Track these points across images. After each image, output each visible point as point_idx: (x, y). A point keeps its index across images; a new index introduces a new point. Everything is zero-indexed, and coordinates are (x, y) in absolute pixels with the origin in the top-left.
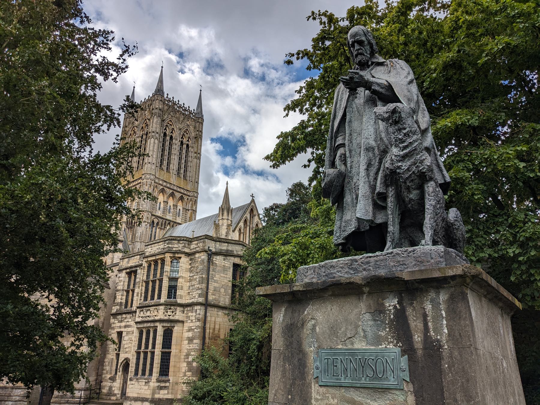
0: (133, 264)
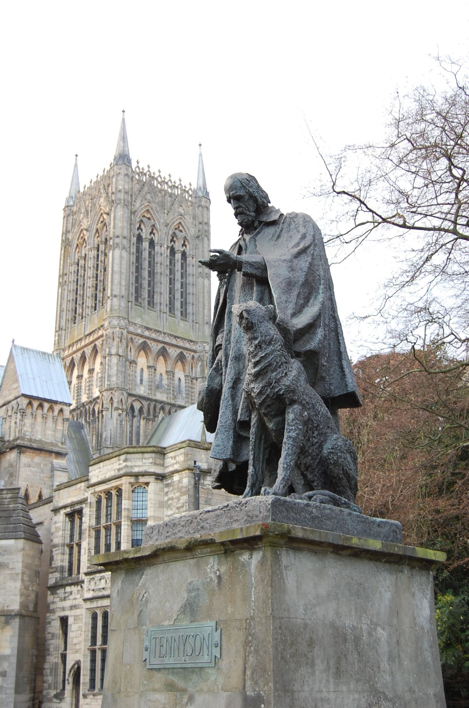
0: (75, 499)
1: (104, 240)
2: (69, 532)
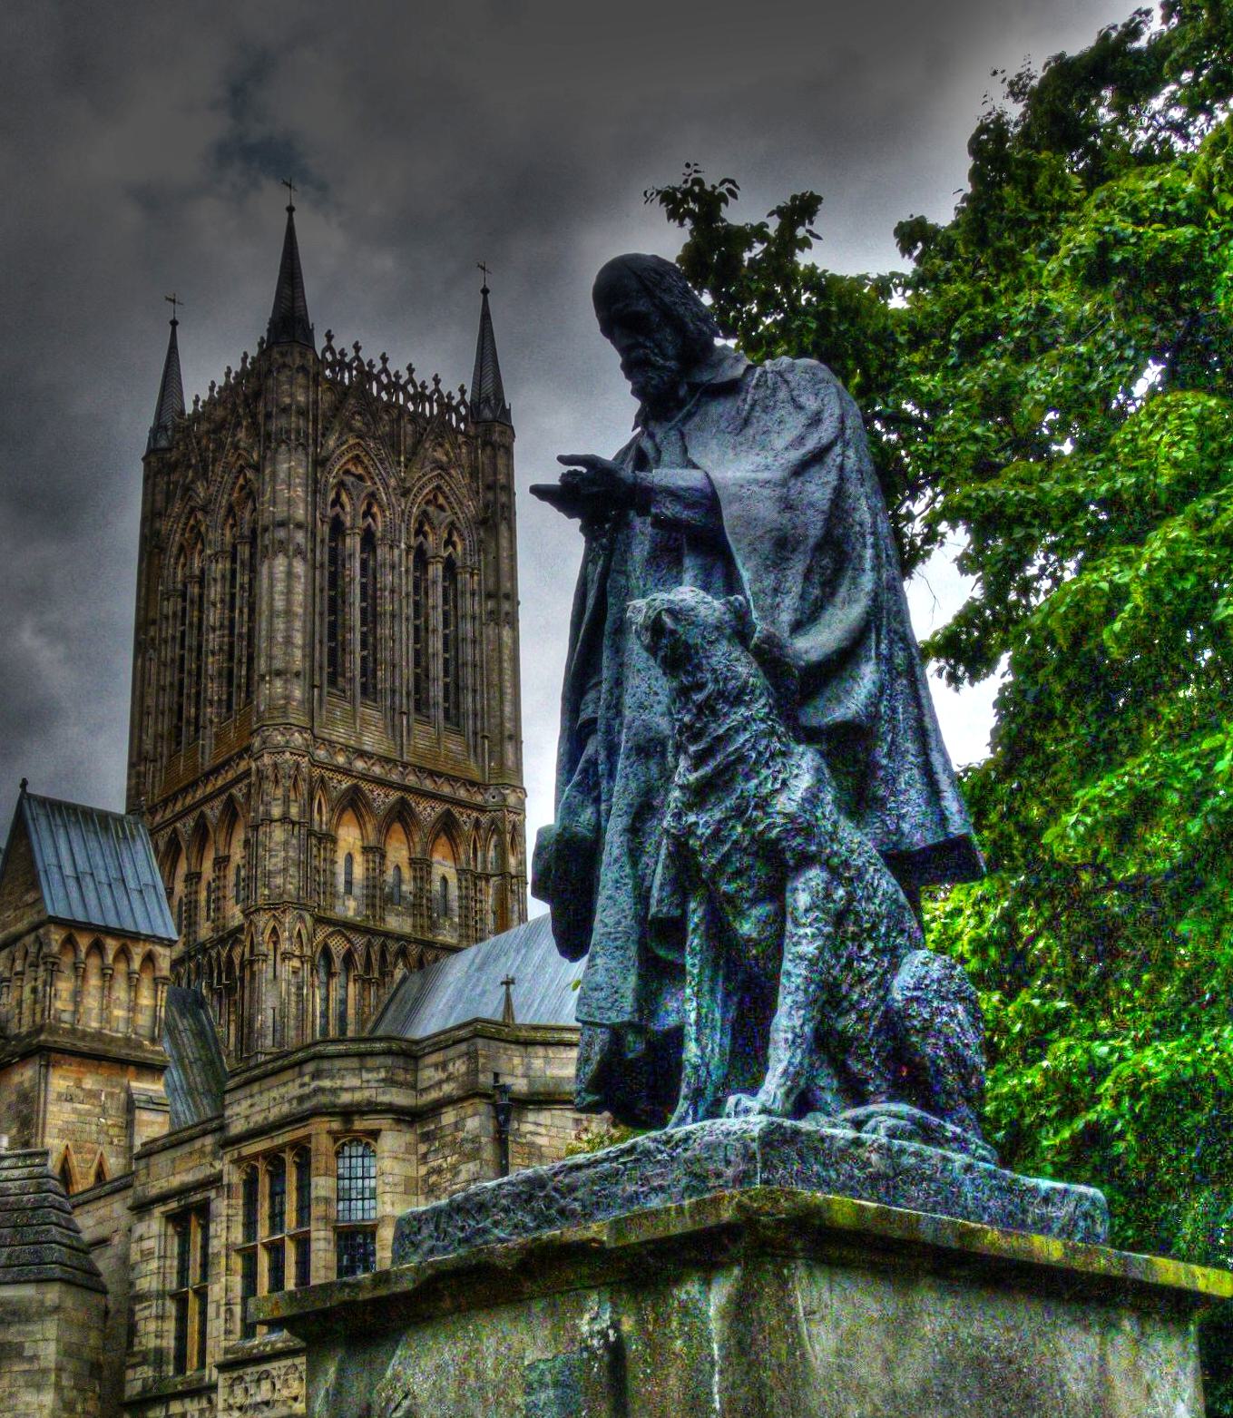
0: (188, 1178)
2: (175, 1263)
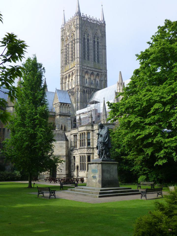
0: (75, 133)
1: (74, 39)
